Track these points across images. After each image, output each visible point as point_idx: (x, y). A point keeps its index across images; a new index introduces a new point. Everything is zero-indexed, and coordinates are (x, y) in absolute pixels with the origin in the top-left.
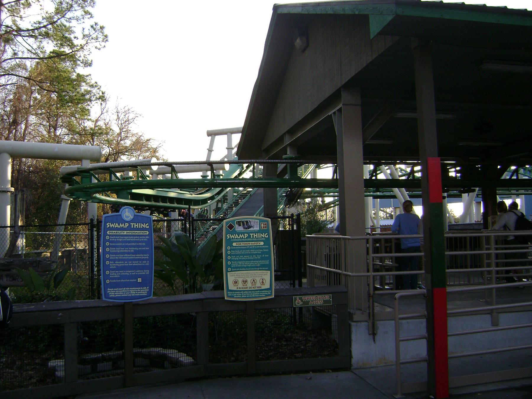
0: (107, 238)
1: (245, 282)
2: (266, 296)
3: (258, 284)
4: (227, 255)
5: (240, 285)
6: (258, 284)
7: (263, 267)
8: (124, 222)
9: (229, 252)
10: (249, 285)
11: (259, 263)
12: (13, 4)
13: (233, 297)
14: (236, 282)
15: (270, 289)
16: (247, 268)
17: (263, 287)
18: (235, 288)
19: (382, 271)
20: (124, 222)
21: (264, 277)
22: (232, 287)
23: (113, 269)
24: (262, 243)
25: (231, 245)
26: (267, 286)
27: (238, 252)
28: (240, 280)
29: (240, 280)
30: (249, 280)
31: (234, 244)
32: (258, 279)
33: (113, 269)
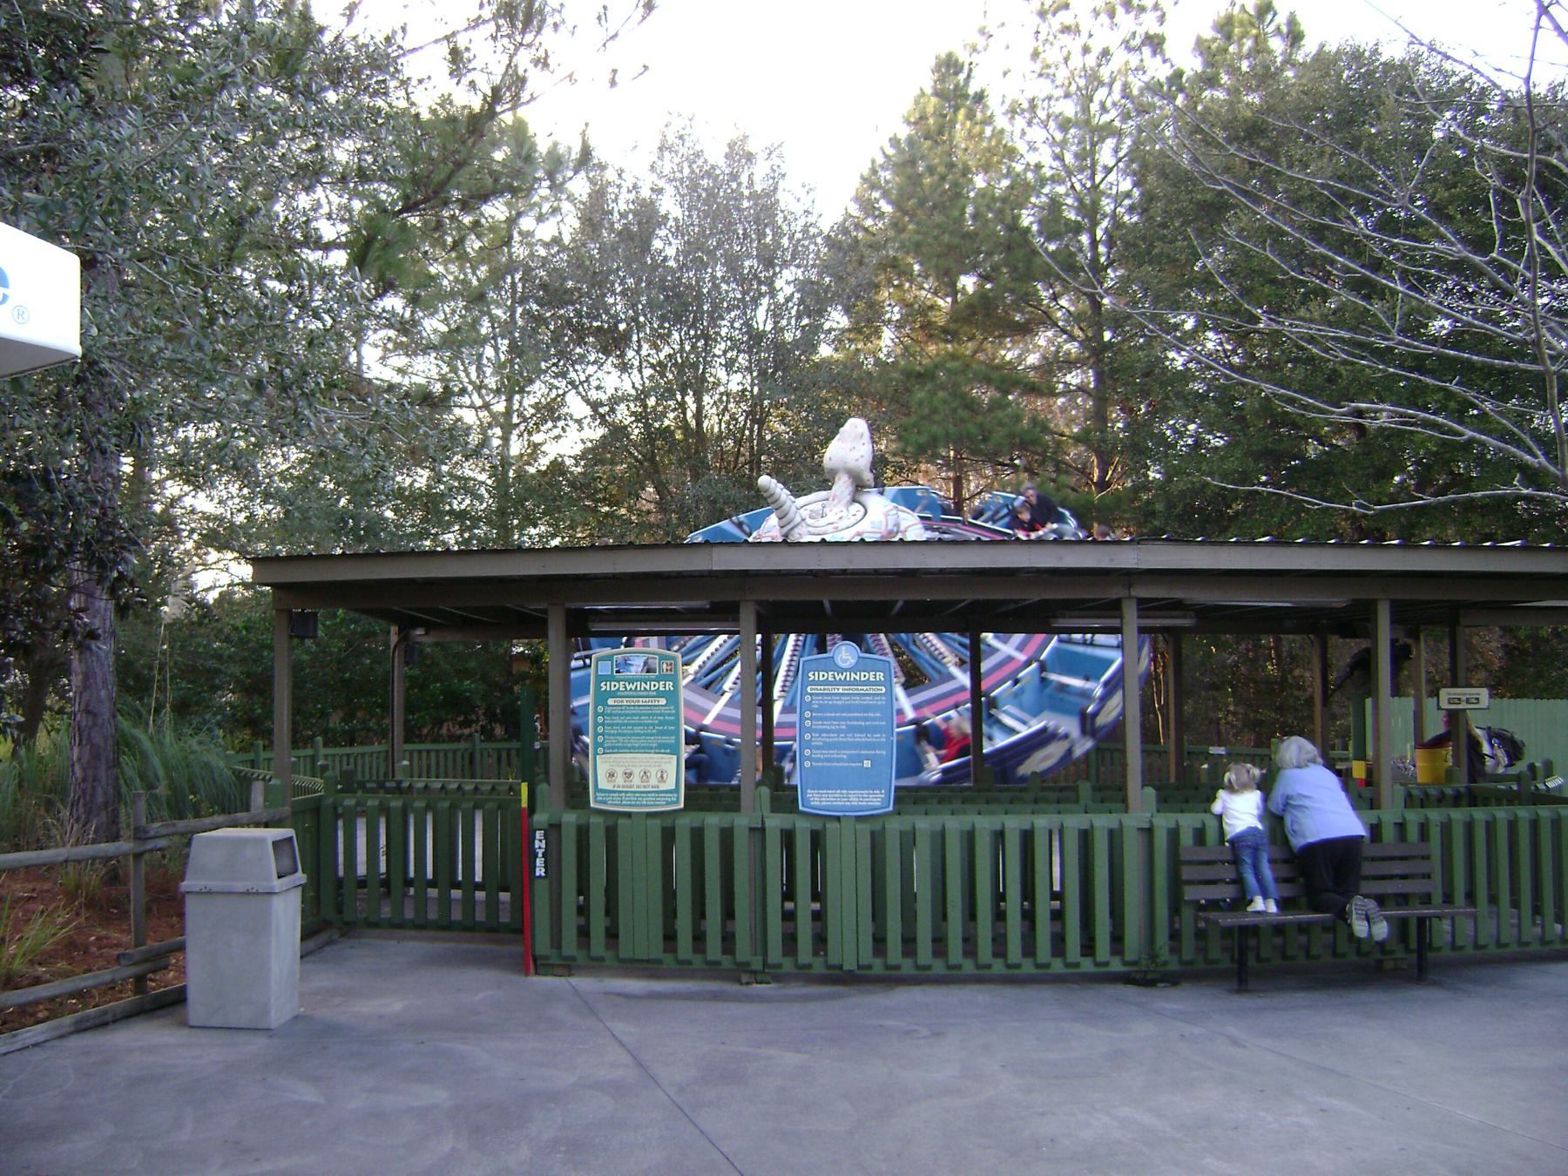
0: (808, 698)
1: (628, 775)
2: (668, 803)
3: (653, 781)
4: (596, 725)
5: (620, 780)
6: (653, 781)
7: (661, 748)
8: (841, 670)
9: (600, 720)
10: (636, 780)
11: (654, 741)
12: (962, 77)
13: (605, 803)
14: (612, 775)
15: (677, 790)
16: (632, 750)
17: (663, 787)
18: (609, 787)
19: (1145, 753)
20: (841, 670)
21: (664, 767)
22: (603, 784)
23: (818, 748)
24: (663, 701)
25: (605, 704)
26: (670, 784)
27: (617, 720)
28: (620, 772)
29: (620, 772)
30: (637, 771)
31: (611, 702)
32: (653, 771)
33: (818, 748)
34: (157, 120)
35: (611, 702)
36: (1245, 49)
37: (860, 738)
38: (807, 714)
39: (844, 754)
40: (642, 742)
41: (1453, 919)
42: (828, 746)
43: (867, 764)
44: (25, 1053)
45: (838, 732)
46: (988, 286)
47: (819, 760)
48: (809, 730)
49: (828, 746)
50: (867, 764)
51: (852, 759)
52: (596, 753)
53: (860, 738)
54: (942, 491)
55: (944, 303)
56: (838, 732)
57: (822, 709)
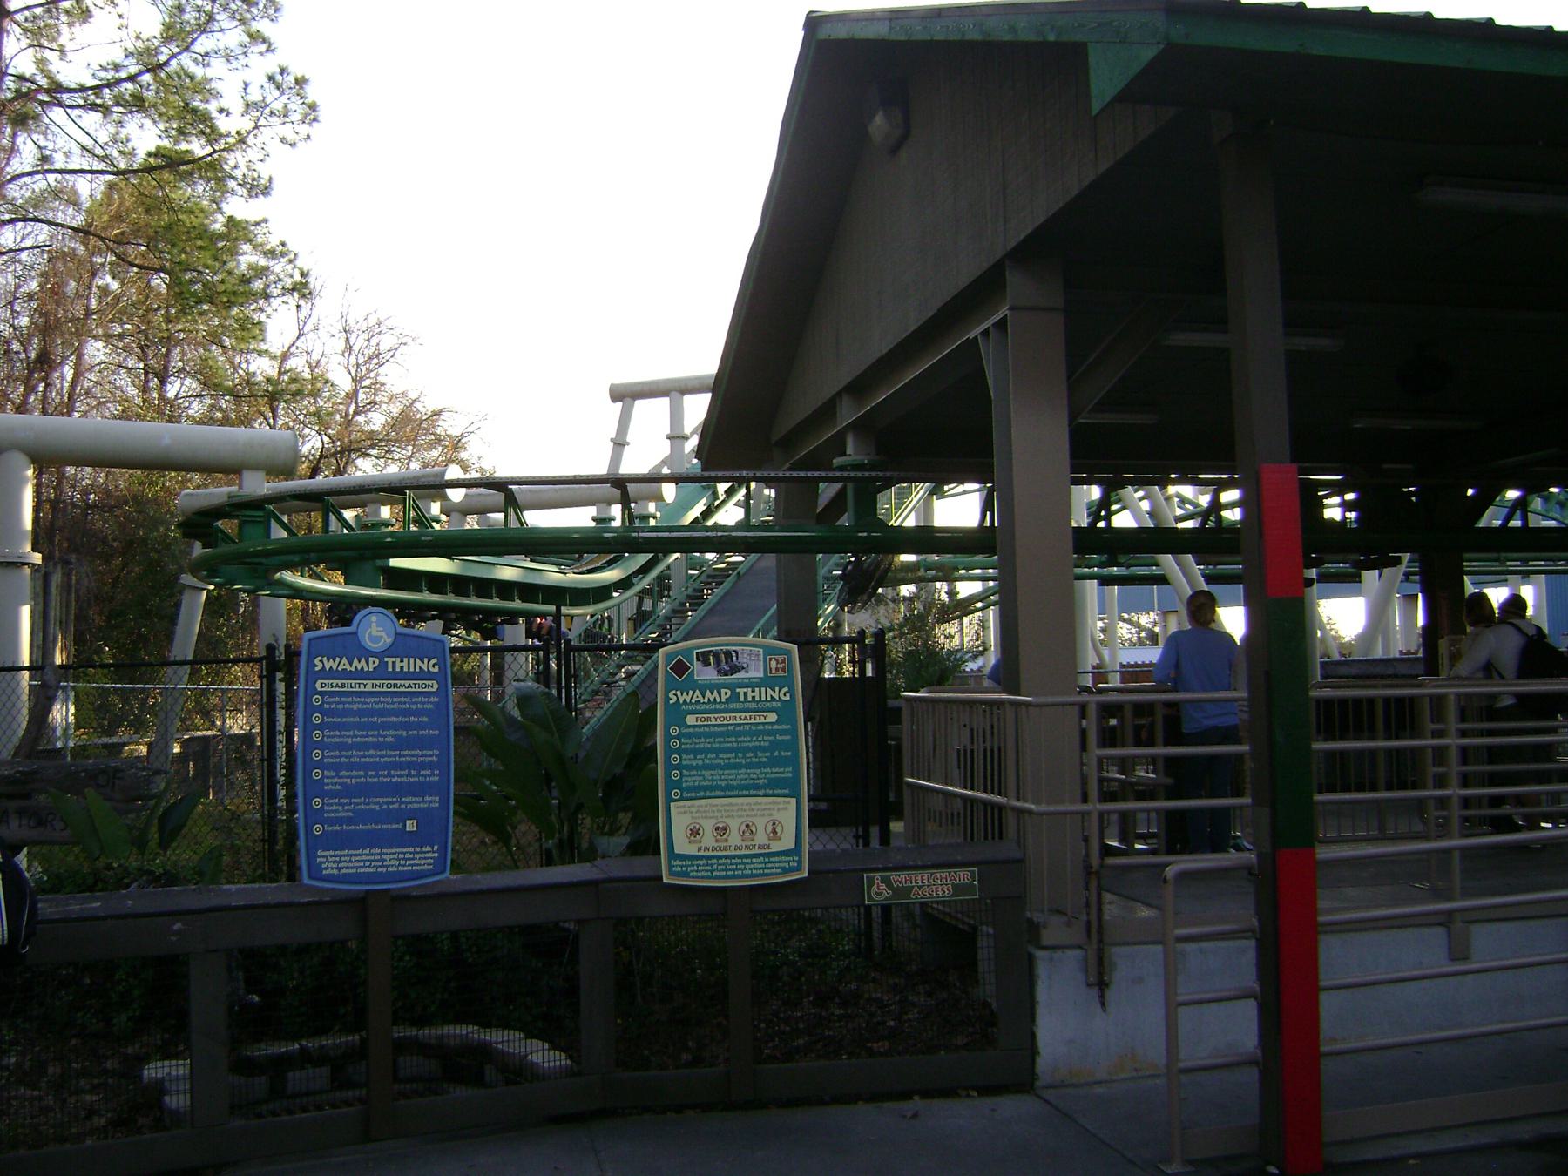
1: (722, 830)
2: (785, 871)
3: (761, 838)
5: (708, 839)
10: (734, 839)
17: (776, 847)
18: (692, 850)
20: (367, 654)
21: (777, 816)
22: (682, 845)
25: (682, 723)
30: (734, 824)
31: (690, 720)
32: (760, 824)
52: (669, 800)
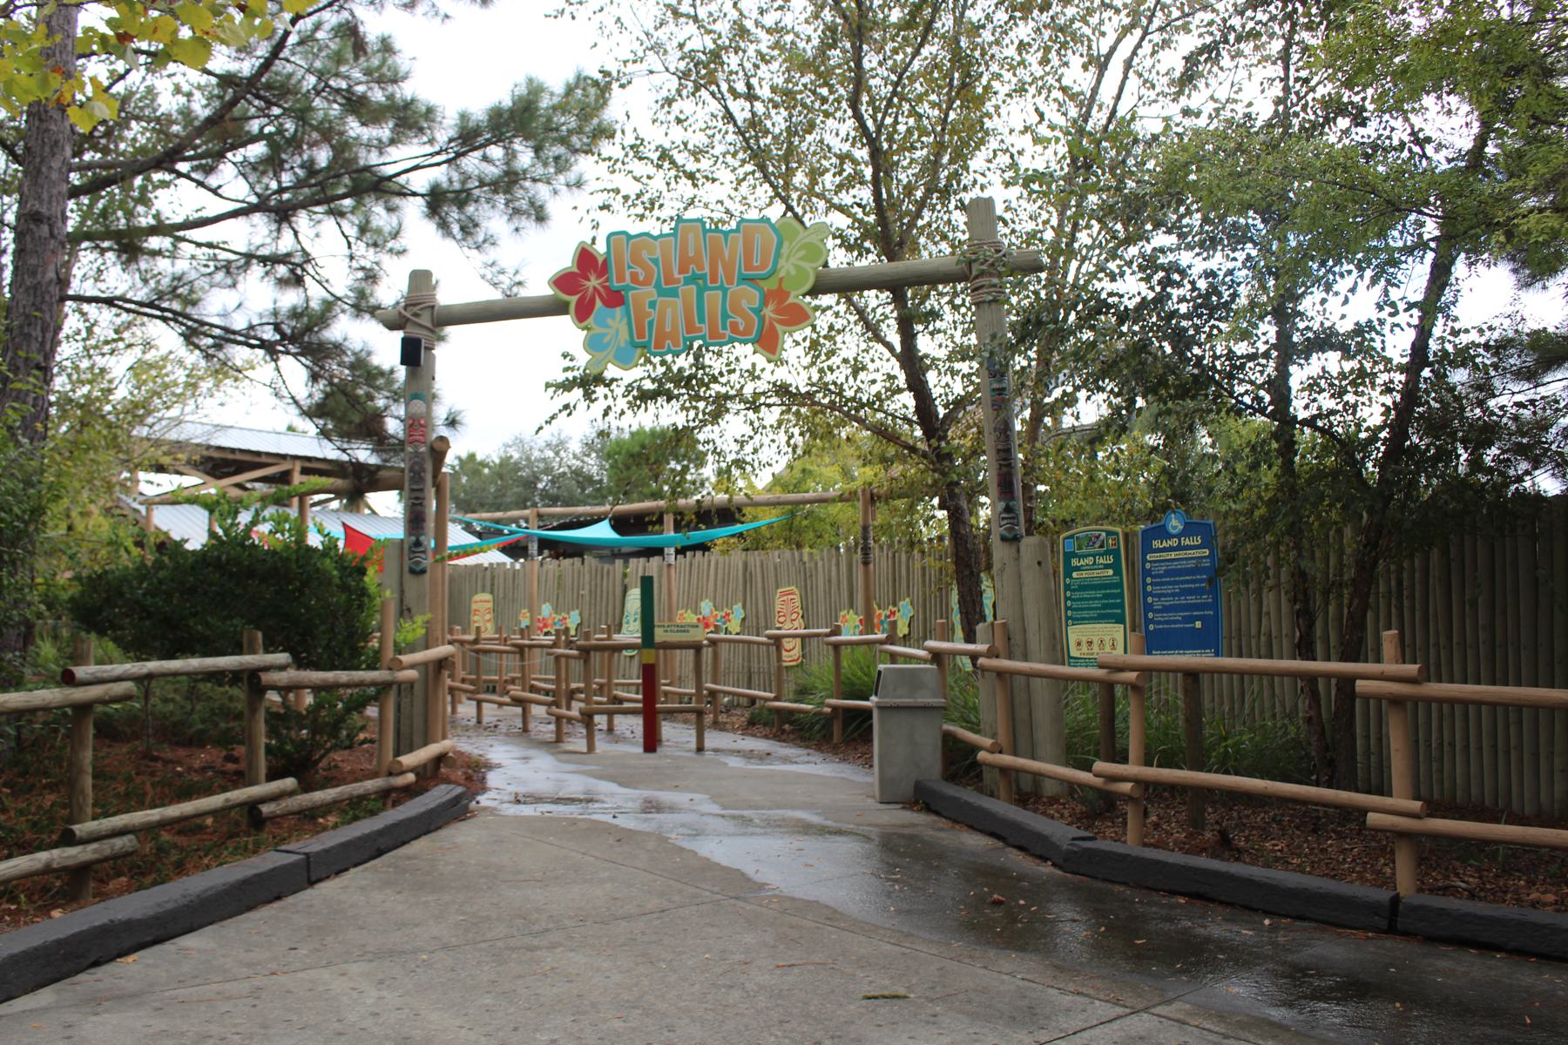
0: (1148, 566)
5: (1084, 648)
10: (1096, 648)
24: (1111, 572)
31: (1075, 575)
34: (172, 700)
35: (1075, 575)
36: (1097, 15)
37: (1192, 600)
38: (1149, 580)
39: (1178, 616)
40: (1093, 613)
41: (479, 722)
42: (1166, 609)
43: (1198, 624)
44: (877, 1002)
45: (1173, 595)
46: (1309, 184)
47: (1159, 623)
48: (1151, 594)
49: (1166, 609)
50: (1198, 624)
51: (1186, 620)
53: (1192, 600)
54: (943, 444)
55: (1422, 22)
56: (1173, 595)
57: (1168, 573)
